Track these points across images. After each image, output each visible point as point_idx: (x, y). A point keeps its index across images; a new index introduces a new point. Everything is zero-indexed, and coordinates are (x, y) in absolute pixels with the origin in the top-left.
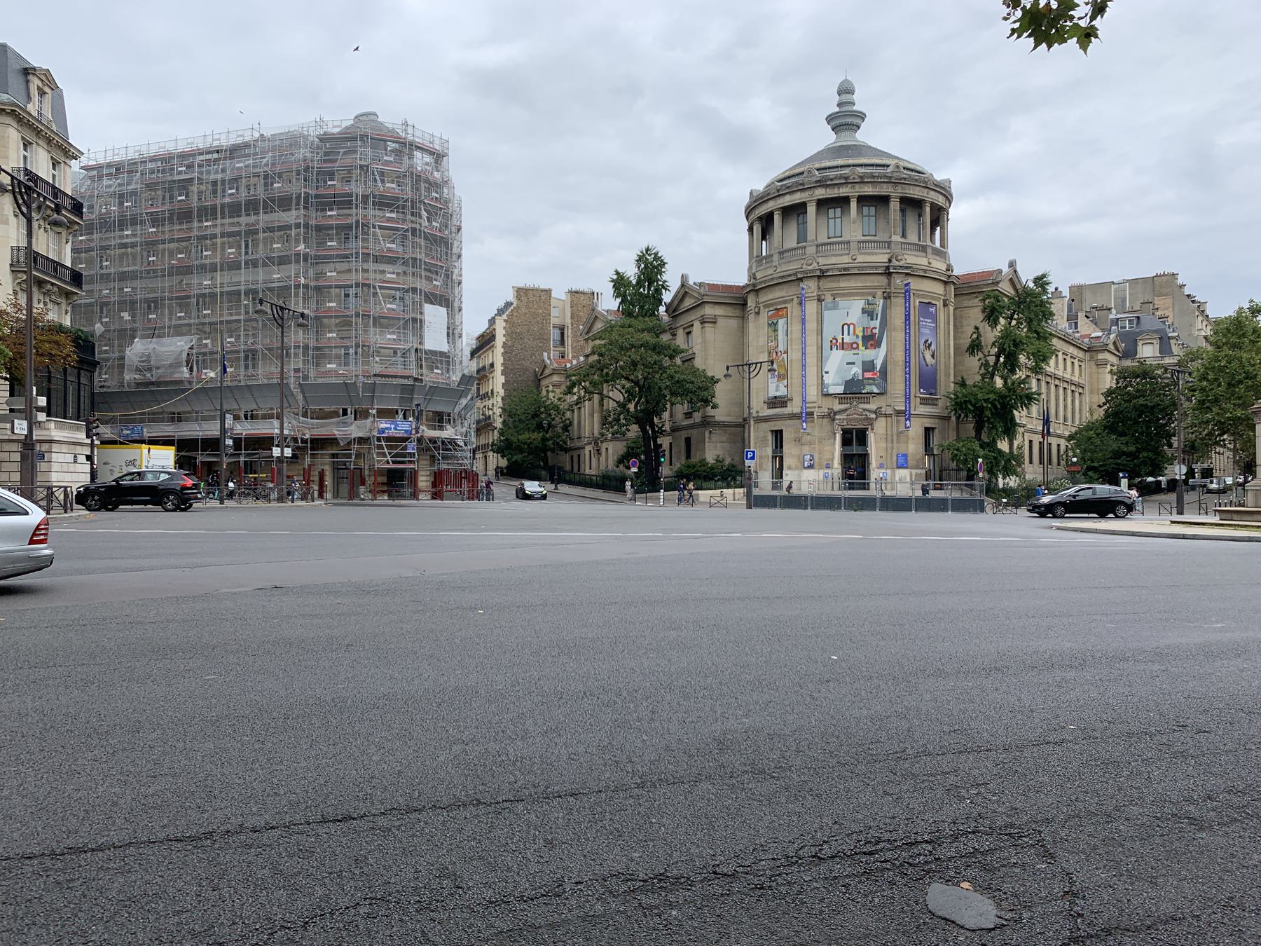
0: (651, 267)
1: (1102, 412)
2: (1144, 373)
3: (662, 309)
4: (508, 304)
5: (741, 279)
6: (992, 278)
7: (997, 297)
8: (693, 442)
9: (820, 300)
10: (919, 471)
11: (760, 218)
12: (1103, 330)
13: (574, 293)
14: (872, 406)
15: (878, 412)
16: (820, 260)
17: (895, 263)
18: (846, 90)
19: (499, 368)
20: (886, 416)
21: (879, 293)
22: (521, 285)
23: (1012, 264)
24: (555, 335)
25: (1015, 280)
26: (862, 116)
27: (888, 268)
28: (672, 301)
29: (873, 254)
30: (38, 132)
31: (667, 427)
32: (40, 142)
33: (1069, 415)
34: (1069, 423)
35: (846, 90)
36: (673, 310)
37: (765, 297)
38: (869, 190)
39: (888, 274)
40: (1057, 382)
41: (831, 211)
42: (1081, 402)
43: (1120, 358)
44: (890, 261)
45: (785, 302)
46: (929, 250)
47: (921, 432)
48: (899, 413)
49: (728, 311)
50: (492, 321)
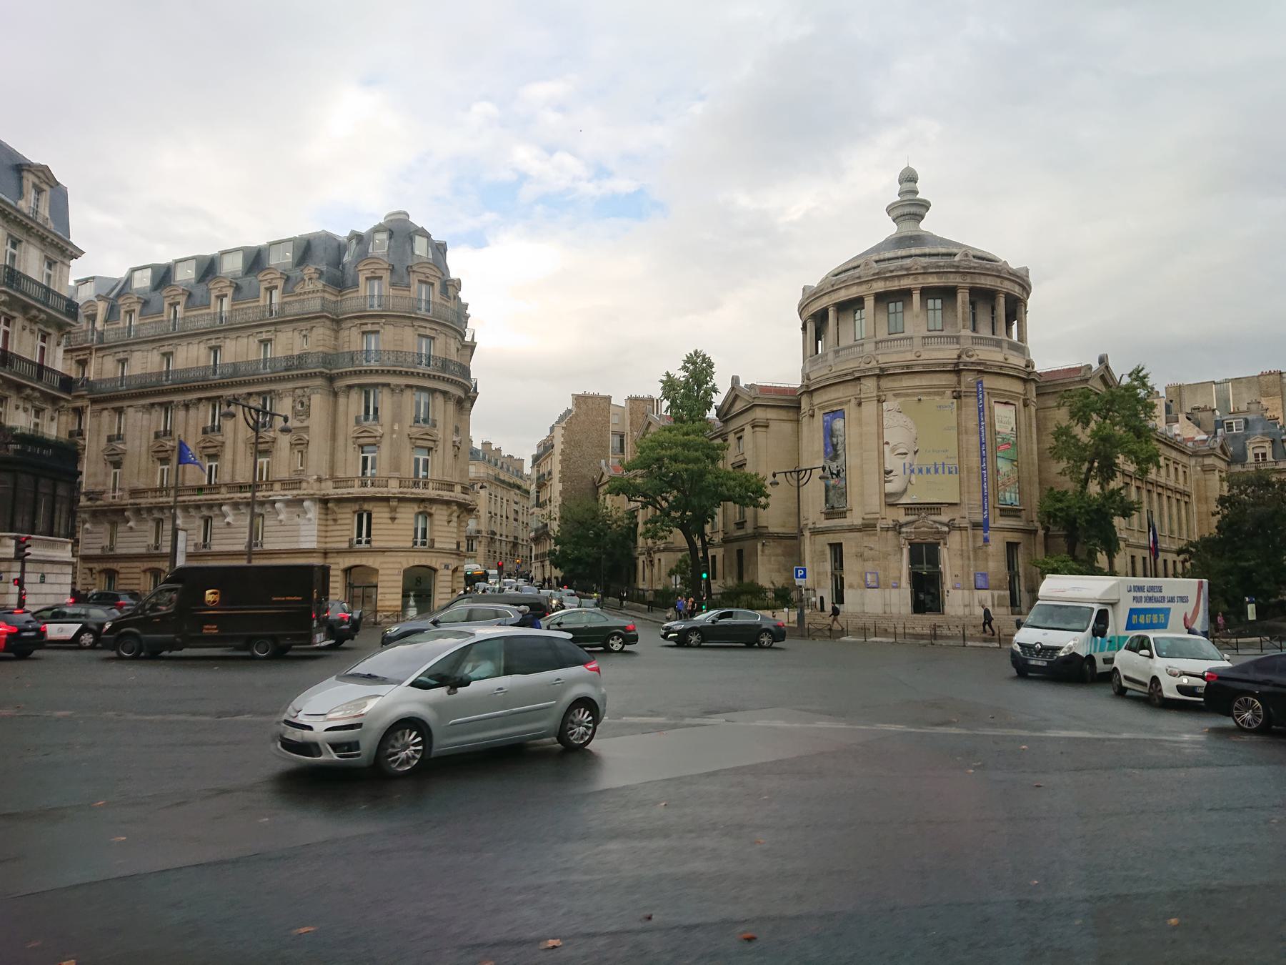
0: (699, 368)
1: (1215, 521)
2: (1261, 481)
3: (711, 414)
4: (569, 411)
5: (796, 382)
6: (1077, 375)
7: (1086, 394)
8: (745, 553)
9: (880, 401)
10: (1002, 592)
11: (814, 316)
12: (1206, 433)
13: (633, 400)
14: (944, 518)
15: (951, 525)
16: (879, 358)
17: (964, 358)
18: (909, 178)
19: (556, 476)
20: (960, 529)
21: (948, 392)
22: (581, 393)
23: (1103, 360)
24: (614, 441)
25: (1108, 377)
26: (925, 205)
27: (957, 364)
28: (723, 404)
29: (939, 350)
30: (28, 229)
31: (717, 538)
32: (31, 240)
33: (1175, 527)
34: (1176, 535)
35: (909, 178)
36: (723, 413)
37: (819, 399)
38: (933, 281)
39: (958, 372)
40: (1160, 490)
41: (892, 306)
42: (1187, 513)
43: (1229, 464)
44: (959, 357)
45: (841, 404)
46: (1005, 345)
47: (1002, 548)
48: (975, 525)
49: (783, 414)
50: (552, 429)
